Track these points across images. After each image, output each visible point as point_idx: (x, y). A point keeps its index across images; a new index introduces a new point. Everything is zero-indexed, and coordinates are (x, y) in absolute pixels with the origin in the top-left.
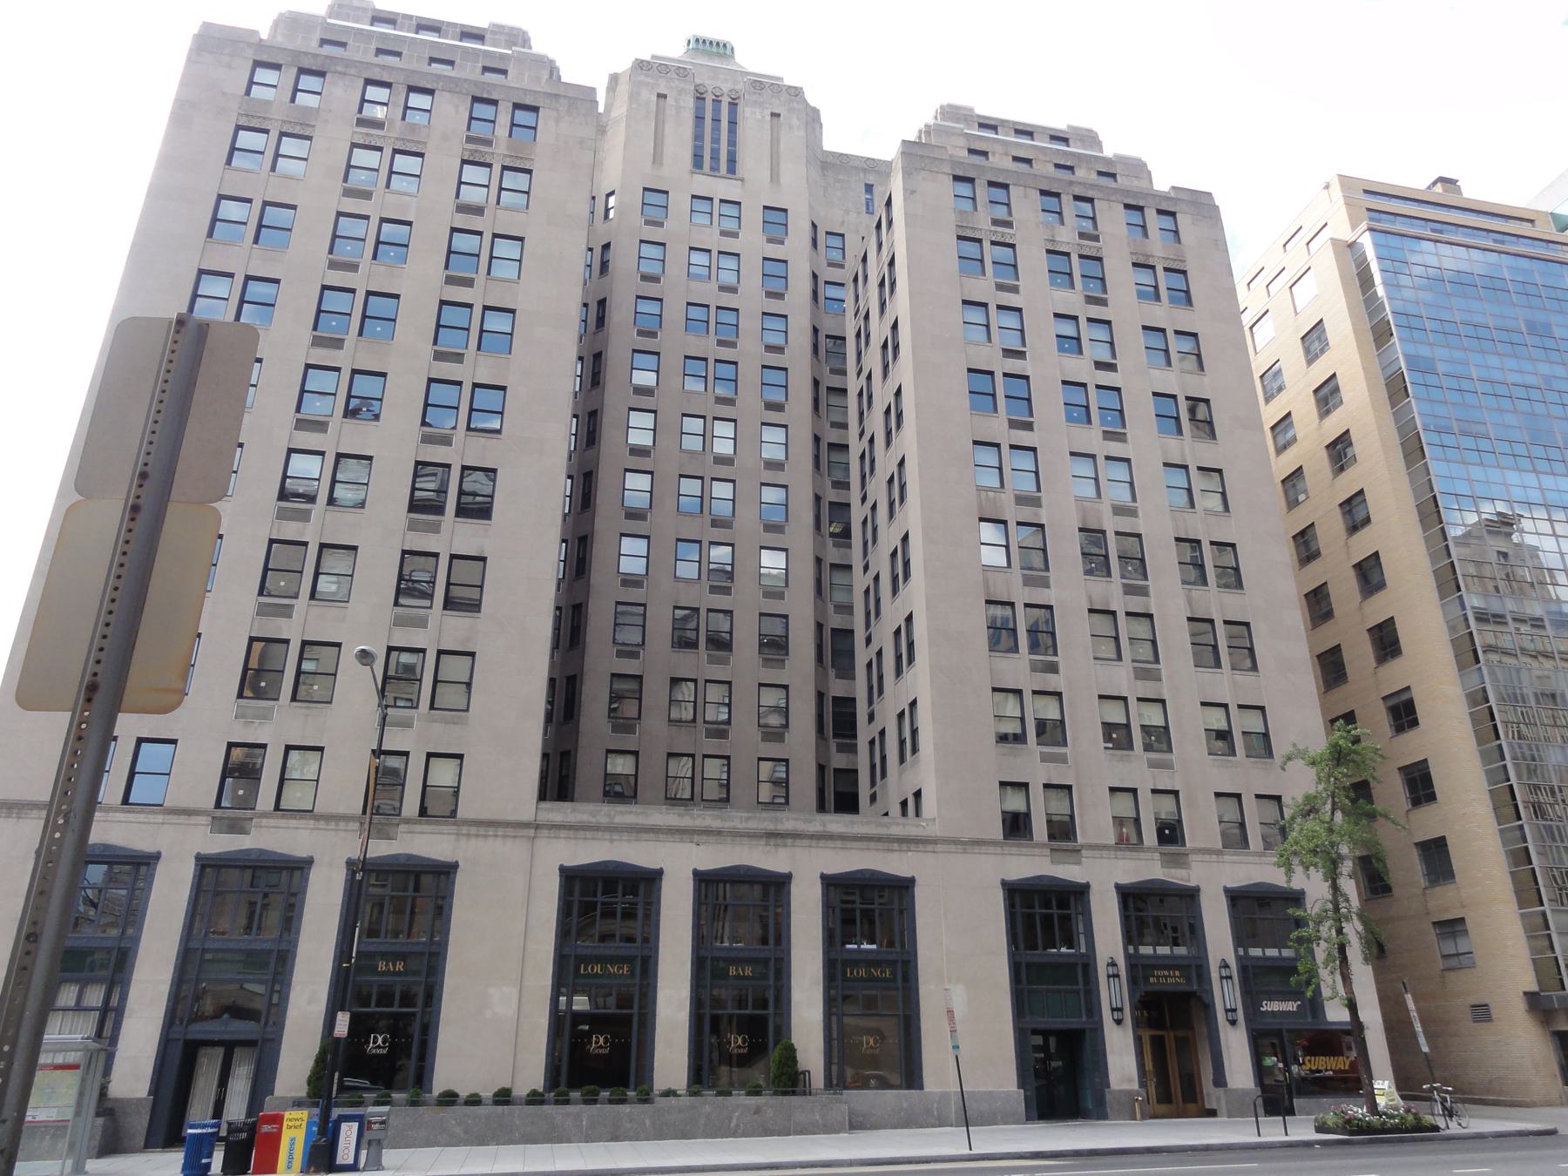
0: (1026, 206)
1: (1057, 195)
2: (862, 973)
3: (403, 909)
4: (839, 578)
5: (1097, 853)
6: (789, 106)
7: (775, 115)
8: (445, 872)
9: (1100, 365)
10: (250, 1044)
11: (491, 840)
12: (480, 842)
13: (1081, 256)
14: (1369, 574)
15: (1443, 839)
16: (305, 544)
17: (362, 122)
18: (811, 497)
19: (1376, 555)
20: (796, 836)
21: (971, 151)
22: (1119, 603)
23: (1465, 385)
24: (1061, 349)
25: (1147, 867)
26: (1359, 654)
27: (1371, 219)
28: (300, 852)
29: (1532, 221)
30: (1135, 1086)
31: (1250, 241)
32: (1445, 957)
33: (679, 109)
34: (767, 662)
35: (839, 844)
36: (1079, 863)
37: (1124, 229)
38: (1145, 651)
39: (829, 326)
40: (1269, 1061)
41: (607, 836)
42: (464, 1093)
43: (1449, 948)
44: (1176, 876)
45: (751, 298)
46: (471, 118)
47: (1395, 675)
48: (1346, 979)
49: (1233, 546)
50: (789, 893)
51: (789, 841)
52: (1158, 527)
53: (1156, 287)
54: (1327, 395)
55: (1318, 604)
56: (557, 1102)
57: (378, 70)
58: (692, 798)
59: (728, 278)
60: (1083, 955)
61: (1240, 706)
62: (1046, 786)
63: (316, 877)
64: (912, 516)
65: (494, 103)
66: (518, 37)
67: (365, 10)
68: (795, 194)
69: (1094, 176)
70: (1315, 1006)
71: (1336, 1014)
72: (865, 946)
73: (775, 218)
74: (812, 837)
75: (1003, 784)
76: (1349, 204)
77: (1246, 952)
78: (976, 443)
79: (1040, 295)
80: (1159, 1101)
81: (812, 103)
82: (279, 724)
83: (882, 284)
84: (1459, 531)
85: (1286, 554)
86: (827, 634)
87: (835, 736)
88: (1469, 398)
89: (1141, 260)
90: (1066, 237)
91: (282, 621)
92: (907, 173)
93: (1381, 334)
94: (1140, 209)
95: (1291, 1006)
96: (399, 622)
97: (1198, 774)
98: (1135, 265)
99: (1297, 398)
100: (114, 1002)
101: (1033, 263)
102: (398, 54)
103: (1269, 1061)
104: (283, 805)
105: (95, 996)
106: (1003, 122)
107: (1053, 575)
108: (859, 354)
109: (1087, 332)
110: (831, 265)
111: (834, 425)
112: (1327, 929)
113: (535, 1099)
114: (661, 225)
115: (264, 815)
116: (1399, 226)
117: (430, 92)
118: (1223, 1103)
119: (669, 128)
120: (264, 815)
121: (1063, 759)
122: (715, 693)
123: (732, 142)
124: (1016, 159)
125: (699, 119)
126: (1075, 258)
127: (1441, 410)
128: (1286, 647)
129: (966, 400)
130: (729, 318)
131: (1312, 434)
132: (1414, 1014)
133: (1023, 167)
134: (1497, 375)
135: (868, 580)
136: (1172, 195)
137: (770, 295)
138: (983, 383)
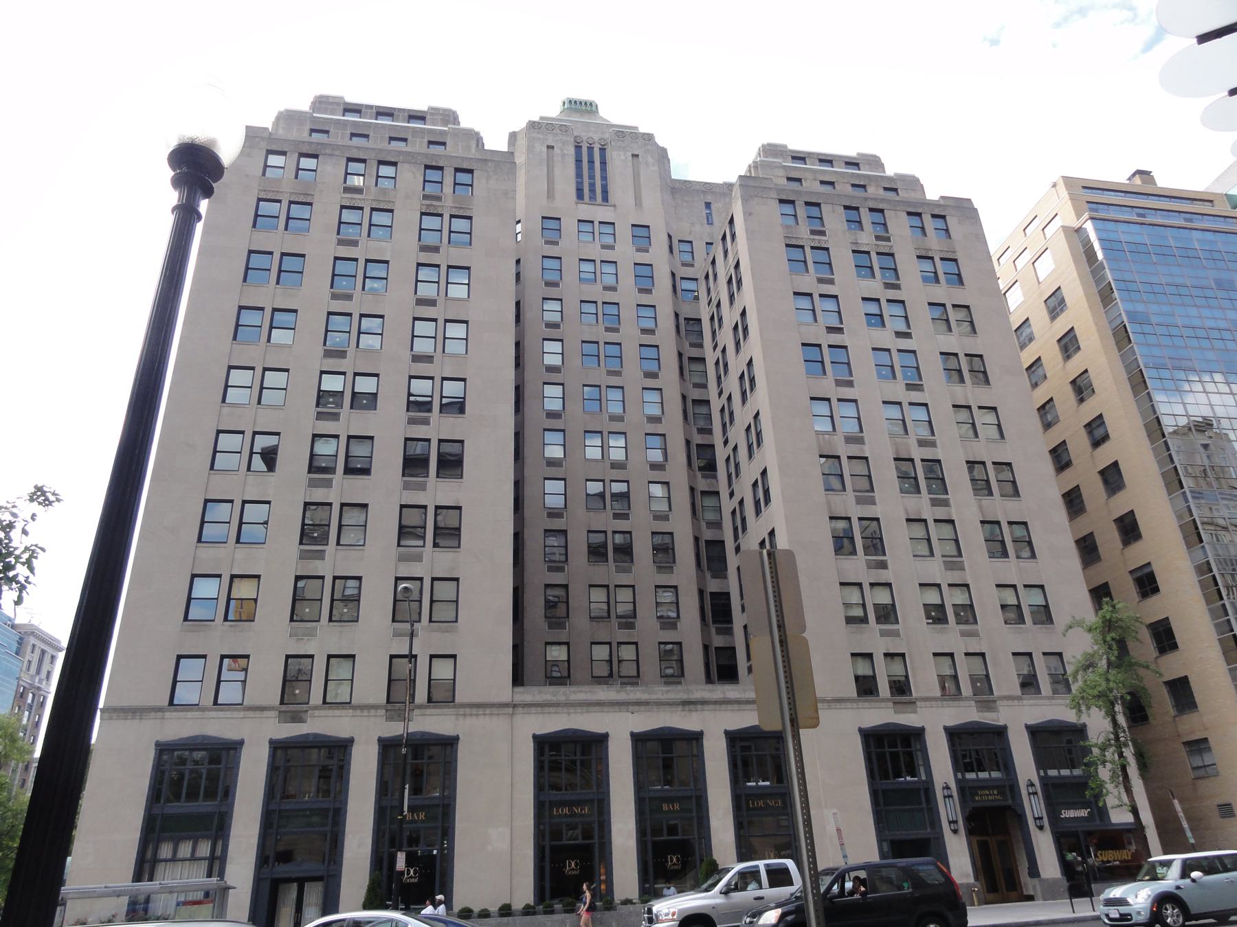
0: (834, 219)
1: (857, 209)
2: (761, 803)
3: (421, 769)
4: (709, 502)
5: (928, 704)
6: (645, 149)
7: (635, 156)
8: (450, 743)
9: (899, 334)
10: (319, 879)
11: (481, 718)
12: (474, 720)
13: (878, 254)
14: (1112, 477)
15: (1186, 677)
16: (330, 504)
17: (347, 190)
18: (683, 442)
19: (1116, 464)
20: (703, 702)
21: (789, 179)
22: (928, 513)
23: (1174, 331)
24: (869, 324)
25: (966, 713)
26: (1109, 539)
27: (1091, 210)
28: (344, 734)
29: (1211, 201)
30: (972, 880)
31: (997, 230)
32: (1194, 769)
33: (563, 156)
34: (660, 569)
35: (736, 707)
36: (915, 712)
37: (909, 231)
38: (950, 549)
39: (687, 311)
40: (1070, 856)
41: (566, 710)
42: (476, 909)
43: (1197, 762)
44: (988, 718)
45: (628, 294)
46: (425, 181)
47: (1138, 554)
48: (1129, 790)
49: (1009, 464)
50: (350, 754)
51: (699, 707)
52: (953, 453)
53: (935, 273)
54: (1068, 344)
55: (1073, 501)
56: (545, 913)
57: (355, 150)
58: (611, 675)
59: (610, 280)
60: (924, 782)
61: (1025, 586)
62: (886, 655)
63: (245, 754)
64: (769, 455)
65: (441, 168)
66: (449, 117)
67: (338, 104)
68: (654, 213)
69: (881, 191)
70: (1103, 813)
71: (1120, 817)
72: (761, 783)
73: (641, 232)
74: (716, 702)
75: (853, 655)
76: (1073, 198)
77: (1046, 773)
78: (812, 399)
79: (851, 285)
80: (989, 891)
81: (661, 145)
82: (324, 639)
83: (730, 281)
84: (1171, 430)
85: (1048, 466)
86: (702, 545)
87: (714, 622)
88: (1179, 342)
89: (923, 253)
90: (866, 239)
91: (318, 563)
92: (745, 201)
93: (1106, 296)
94: (919, 215)
95: (1083, 813)
96: (402, 558)
97: (998, 639)
98: (919, 257)
99: (1045, 345)
100: (218, 852)
101: (843, 260)
102: (367, 136)
103: (1070, 856)
104: (328, 700)
105: (204, 849)
106: (810, 154)
107: (877, 494)
108: (714, 333)
109: (887, 310)
110: (684, 265)
111: (696, 386)
112: (1110, 754)
113: (528, 911)
114: (556, 243)
115: (316, 708)
116: (1113, 214)
117: (394, 164)
118: (1039, 889)
119: (557, 172)
120: (316, 708)
121: (896, 634)
122: (624, 595)
123: (604, 178)
124: (822, 182)
125: (579, 161)
126: (873, 255)
127: (1156, 352)
128: (1055, 536)
129: (802, 366)
130: (612, 310)
131: (1059, 374)
132: (1181, 814)
133: (828, 188)
134: (1197, 322)
135: (735, 503)
136: (942, 202)
137: (641, 291)
138: (814, 353)
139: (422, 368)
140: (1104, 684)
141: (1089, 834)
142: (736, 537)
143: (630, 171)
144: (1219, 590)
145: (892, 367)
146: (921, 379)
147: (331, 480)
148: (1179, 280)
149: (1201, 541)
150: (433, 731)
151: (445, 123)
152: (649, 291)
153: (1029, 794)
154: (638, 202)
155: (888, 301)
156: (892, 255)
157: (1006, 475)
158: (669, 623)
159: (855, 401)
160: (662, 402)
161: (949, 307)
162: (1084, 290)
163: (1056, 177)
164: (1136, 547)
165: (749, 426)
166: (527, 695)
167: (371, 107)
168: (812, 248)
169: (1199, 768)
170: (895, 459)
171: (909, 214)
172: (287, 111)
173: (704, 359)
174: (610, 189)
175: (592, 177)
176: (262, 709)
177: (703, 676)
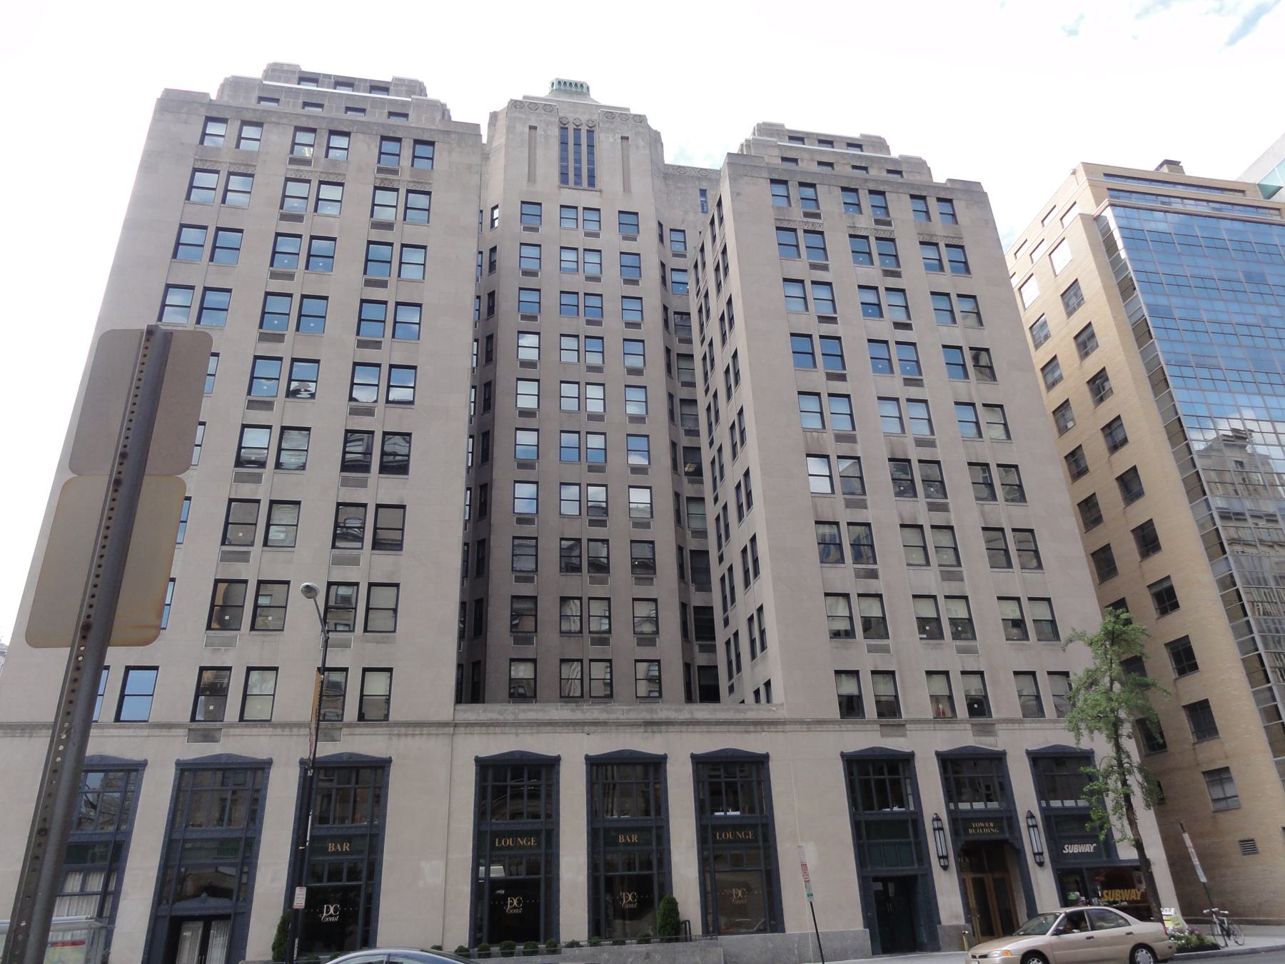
0: (830, 201)
1: (856, 190)
2: (729, 836)
3: (346, 797)
4: (694, 509)
6: (636, 131)
7: (624, 138)
8: (381, 767)
9: (898, 325)
10: (225, 917)
13: (877, 239)
14: (1130, 484)
18: (668, 443)
19: (1134, 469)
20: (669, 723)
21: (784, 159)
22: (925, 518)
23: (1199, 326)
24: (866, 314)
25: (961, 736)
26: (1126, 551)
27: (1111, 197)
28: (262, 756)
29: (1243, 192)
30: (962, 922)
31: (1013, 218)
32: (1214, 800)
33: (547, 137)
34: (639, 581)
35: (704, 728)
36: (904, 735)
37: (912, 214)
38: (949, 557)
39: (676, 304)
43: (1218, 793)
45: (612, 285)
47: (1157, 567)
48: (1133, 823)
49: (1016, 467)
53: (940, 260)
54: (1085, 340)
55: (1089, 511)
58: (582, 696)
59: (593, 270)
60: (912, 813)
62: (874, 672)
63: (670, 768)
64: (751, 455)
65: (399, 140)
66: (416, 88)
67: (293, 72)
68: (643, 199)
69: (884, 174)
70: (1108, 846)
71: (1126, 853)
72: (731, 813)
73: (629, 219)
74: (682, 723)
75: (838, 672)
76: (1093, 185)
77: (1048, 804)
79: (846, 271)
82: (242, 650)
83: (717, 269)
85: (1059, 471)
87: (697, 639)
88: (1204, 338)
89: (927, 239)
90: (865, 223)
93: (1126, 289)
94: (923, 198)
95: (1088, 848)
96: (337, 562)
97: (999, 657)
98: (921, 243)
99: (1061, 343)
100: (112, 887)
101: (839, 245)
105: (96, 883)
106: (809, 135)
108: (702, 325)
109: (886, 299)
110: (675, 255)
111: (685, 384)
113: (461, 953)
114: (536, 230)
115: (231, 725)
116: (1135, 201)
117: (347, 134)
119: (540, 153)
120: (231, 725)
121: (886, 650)
123: (591, 162)
124: (820, 163)
125: (564, 143)
126: (872, 240)
127: (1179, 348)
128: (1065, 547)
129: (790, 358)
131: (1075, 373)
132: (1192, 850)
133: (827, 169)
135: (718, 509)
137: (627, 282)
138: (803, 345)
139: (369, 355)
140: (1104, 704)
141: (1095, 871)
142: (720, 546)
143: (619, 154)
144: (1243, 605)
145: (889, 360)
146: (920, 374)
147: (260, 475)
148: (1205, 273)
149: (1224, 552)
150: (370, 754)
151: (409, 94)
152: (635, 282)
153: (1029, 827)
154: (627, 187)
155: (887, 289)
156: (893, 240)
157: (1013, 479)
158: (647, 640)
159: (848, 396)
160: (645, 403)
161: (954, 297)
162: (1103, 281)
163: (1076, 164)
164: (1156, 559)
165: (733, 425)
166: (472, 712)
167: (329, 76)
168: (805, 231)
169: (1219, 800)
170: (890, 460)
171: (913, 197)
172: (234, 77)
173: (692, 356)
174: (597, 173)
175: (578, 161)
176: (169, 726)
177: (683, 697)
